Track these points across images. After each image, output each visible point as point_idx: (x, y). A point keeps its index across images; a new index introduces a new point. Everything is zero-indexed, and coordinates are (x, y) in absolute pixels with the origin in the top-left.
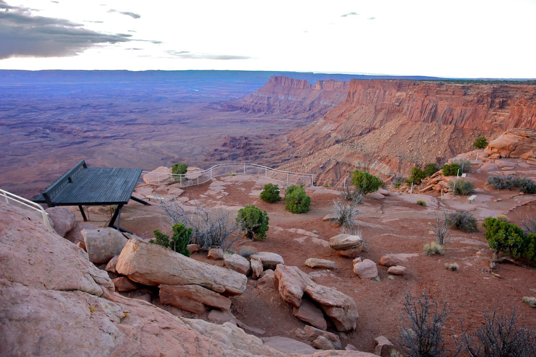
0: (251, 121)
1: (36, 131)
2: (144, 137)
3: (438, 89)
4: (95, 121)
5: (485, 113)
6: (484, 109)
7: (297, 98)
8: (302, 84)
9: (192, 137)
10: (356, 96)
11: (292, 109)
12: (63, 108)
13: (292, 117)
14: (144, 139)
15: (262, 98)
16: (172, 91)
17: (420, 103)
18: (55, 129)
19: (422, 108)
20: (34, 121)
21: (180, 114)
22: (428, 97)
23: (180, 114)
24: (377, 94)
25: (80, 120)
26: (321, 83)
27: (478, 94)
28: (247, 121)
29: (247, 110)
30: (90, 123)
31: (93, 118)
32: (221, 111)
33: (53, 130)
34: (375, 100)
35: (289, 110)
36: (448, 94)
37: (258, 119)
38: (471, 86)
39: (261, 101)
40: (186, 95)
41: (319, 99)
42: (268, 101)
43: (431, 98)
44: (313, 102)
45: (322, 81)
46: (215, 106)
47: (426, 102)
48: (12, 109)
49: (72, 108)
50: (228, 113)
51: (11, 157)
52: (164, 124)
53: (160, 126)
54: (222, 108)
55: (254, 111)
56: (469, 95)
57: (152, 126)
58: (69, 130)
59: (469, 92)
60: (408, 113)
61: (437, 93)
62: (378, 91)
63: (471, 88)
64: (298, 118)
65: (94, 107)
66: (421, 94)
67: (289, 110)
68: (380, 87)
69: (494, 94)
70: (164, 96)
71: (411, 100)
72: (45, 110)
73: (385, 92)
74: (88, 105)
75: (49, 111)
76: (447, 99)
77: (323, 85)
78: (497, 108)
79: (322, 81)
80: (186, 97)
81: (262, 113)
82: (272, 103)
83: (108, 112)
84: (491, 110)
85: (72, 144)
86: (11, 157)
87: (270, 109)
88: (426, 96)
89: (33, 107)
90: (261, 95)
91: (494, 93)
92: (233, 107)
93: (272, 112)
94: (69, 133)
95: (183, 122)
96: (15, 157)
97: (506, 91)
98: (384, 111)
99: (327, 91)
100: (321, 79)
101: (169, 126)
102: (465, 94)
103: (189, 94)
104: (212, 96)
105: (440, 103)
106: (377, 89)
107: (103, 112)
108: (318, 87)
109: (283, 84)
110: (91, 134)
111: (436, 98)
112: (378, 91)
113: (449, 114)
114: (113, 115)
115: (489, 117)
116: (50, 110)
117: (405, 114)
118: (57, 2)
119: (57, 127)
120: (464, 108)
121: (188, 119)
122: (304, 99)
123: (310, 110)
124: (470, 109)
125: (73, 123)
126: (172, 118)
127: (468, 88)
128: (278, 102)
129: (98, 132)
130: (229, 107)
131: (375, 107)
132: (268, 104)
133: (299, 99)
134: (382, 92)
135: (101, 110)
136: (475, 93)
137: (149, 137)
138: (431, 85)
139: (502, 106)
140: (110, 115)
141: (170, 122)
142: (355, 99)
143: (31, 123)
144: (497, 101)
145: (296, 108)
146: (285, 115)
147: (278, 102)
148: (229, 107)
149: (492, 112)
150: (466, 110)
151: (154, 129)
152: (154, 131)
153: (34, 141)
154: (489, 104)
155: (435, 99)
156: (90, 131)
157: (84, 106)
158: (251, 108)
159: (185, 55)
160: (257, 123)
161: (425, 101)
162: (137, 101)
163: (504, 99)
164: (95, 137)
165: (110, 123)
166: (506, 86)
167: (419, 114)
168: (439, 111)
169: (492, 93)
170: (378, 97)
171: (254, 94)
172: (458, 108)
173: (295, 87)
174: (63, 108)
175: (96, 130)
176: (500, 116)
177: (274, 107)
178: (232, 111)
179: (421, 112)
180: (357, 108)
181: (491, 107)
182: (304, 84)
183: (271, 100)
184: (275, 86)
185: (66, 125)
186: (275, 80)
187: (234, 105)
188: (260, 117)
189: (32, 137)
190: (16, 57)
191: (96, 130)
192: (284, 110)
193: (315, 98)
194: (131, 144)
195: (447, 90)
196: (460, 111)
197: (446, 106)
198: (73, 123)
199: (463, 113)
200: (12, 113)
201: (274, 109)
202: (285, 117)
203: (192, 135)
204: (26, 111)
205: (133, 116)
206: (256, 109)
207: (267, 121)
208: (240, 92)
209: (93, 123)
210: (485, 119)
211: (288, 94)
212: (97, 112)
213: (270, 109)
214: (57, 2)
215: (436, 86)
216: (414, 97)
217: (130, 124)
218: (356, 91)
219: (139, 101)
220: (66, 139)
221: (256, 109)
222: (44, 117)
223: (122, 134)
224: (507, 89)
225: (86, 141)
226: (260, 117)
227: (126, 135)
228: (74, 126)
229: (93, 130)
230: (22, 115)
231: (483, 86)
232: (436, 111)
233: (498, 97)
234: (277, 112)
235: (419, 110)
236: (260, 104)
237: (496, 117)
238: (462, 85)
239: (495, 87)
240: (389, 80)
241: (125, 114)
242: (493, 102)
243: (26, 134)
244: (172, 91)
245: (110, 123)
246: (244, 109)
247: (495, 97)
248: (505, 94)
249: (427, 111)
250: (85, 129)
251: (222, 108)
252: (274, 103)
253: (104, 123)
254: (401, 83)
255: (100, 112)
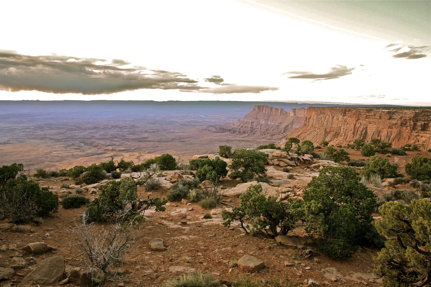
0: (235, 141)
1: (73, 144)
2: (148, 151)
3: (367, 114)
4: (118, 138)
5: (409, 134)
6: (407, 131)
7: (275, 123)
8: (279, 112)
9: (185, 152)
10: (311, 120)
11: (270, 132)
12: (98, 128)
13: (269, 138)
14: (148, 153)
15: (247, 123)
16: (183, 117)
17: (352, 126)
18: (87, 144)
19: (354, 130)
20: (75, 137)
21: (182, 134)
22: (359, 121)
23: (182, 134)
24: (327, 119)
25: (107, 137)
26: (294, 110)
27: (401, 118)
28: (232, 140)
29: (235, 132)
30: (113, 139)
31: (116, 136)
32: (215, 132)
33: (86, 144)
34: (325, 124)
35: (268, 132)
36: (375, 119)
37: (242, 139)
38: (396, 112)
39: (246, 125)
40: (192, 120)
41: (292, 123)
42: (252, 125)
43: (361, 122)
44: (287, 126)
45: (295, 109)
46: (210, 129)
47: (358, 125)
48: (63, 128)
49: (105, 128)
50: (219, 134)
51: (48, 163)
52: (167, 142)
53: (164, 143)
54: (216, 130)
55: (240, 132)
56: (393, 119)
57: (157, 143)
58: (96, 144)
59: (395, 116)
60: (343, 135)
61: (367, 117)
62: (327, 117)
63: (396, 113)
64: (274, 138)
65: (120, 128)
66: (353, 119)
67: (268, 132)
68: (329, 113)
69: (416, 118)
70: (175, 120)
71: (346, 124)
72: (85, 129)
73: (333, 117)
74: (117, 126)
75: (88, 130)
76: (375, 123)
77: (296, 112)
78: (420, 130)
79: (295, 109)
80: (192, 121)
81: (246, 135)
82: (254, 127)
83: (129, 132)
84: (413, 131)
85: (94, 155)
86: (48, 163)
87: (253, 131)
88: (357, 120)
89: (77, 127)
90: (246, 120)
91: (416, 117)
92: (224, 129)
93: (254, 134)
94: (96, 146)
95: (183, 140)
96: (51, 163)
97: (427, 115)
98: (332, 133)
99: (299, 117)
100: (294, 108)
101: (170, 143)
102: (390, 118)
103: (195, 119)
104: (212, 121)
105: (369, 126)
106: (327, 115)
107: (126, 131)
108: (292, 114)
109: (264, 112)
110: (110, 148)
111: (366, 122)
112: (327, 117)
113: (377, 135)
114: (132, 134)
115: (412, 137)
116: (89, 129)
117: (342, 136)
118: (361, 65)
119: (88, 142)
120: (390, 130)
121: (187, 138)
122: (280, 123)
123: (284, 132)
124: (395, 131)
125: (102, 139)
126: (175, 137)
127: (394, 113)
128: (259, 126)
129: (116, 146)
130: (220, 129)
131: (325, 129)
132: (252, 128)
133: (276, 124)
134: (331, 117)
135: (125, 130)
136: (399, 117)
137: (153, 151)
138: (361, 111)
139: (424, 128)
140: (129, 134)
141: (173, 140)
142: (310, 123)
143: (72, 138)
144: (419, 124)
145: (273, 130)
146: (264, 136)
147: (259, 126)
148: (220, 129)
149: (414, 133)
150: (391, 132)
151: (158, 145)
152: (157, 147)
153: (69, 151)
154: (412, 127)
155: (364, 122)
156: (111, 145)
157: (113, 126)
158: (238, 130)
159: (380, 97)
160: (239, 142)
161: (357, 124)
162: (154, 124)
163: (425, 122)
164: (112, 150)
165: (127, 140)
166: (428, 111)
167: (352, 135)
168: (369, 133)
169: (414, 117)
170: (328, 121)
171: (241, 119)
172: (385, 130)
173: (274, 113)
174: (98, 128)
175: (115, 145)
176: (422, 137)
177: (256, 130)
178: (222, 132)
179: (354, 133)
180: (311, 131)
181: (414, 129)
182: (281, 112)
183: (254, 124)
184: (258, 113)
185: (94, 140)
186: (258, 109)
187: (225, 128)
188: (243, 138)
189: (69, 149)
190: (323, 102)
191: (115, 145)
192: (264, 132)
193: (289, 123)
194: (137, 156)
195: (375, 115)
196: (386, 133)
197: (374, 128)
198: (102, 139)
199: (389, 134)
200: (60, 131)
201: (256, 132)
202: (264, 138)
203: (186, 150)
204: (72, 130)
205: (146, 135)
206: (242, 131)
207: (248, 141)
208: (235, 118)
209: (115, 139)
210: (409, 139)
211: (268, 120)
212: (121, 131)
213: (253, 131)
214: (361, 65)
215: (365, 111)
216: (348, 121)
217: (142, 141)
218: (311, 117)
219: (155, 124)
220: (94, 150)
221: (242, 131)
222: (82, 134)
223: (133, 148)
224: (429, 114)
225: (105, 153)
226: (243, 138)
227: (136, 149)
228: (100, 142)
229: (113, 145)
230: (69, 132)
231: (406, 111)
232: (366, 133)
233: (420, 120)
234: (258, 134)
235: (351, 132)
236: (245, 127)
237: (418, 138)
238: (388, 111)
239: (417, 112)
240: (336, 107)
241: (141, 133)
242: (415, 125)
243: (65, 146)
244: (183, 117)
245: (127, 140)
246: (232, 131)
247: (417, 121)
248: (426, 118)
249: (359, 133)
250: (108, 144)
251: (216, 130)
252: (256, 126)
253: (123, 140)
254: (370, 109)
255: (124, 132)
